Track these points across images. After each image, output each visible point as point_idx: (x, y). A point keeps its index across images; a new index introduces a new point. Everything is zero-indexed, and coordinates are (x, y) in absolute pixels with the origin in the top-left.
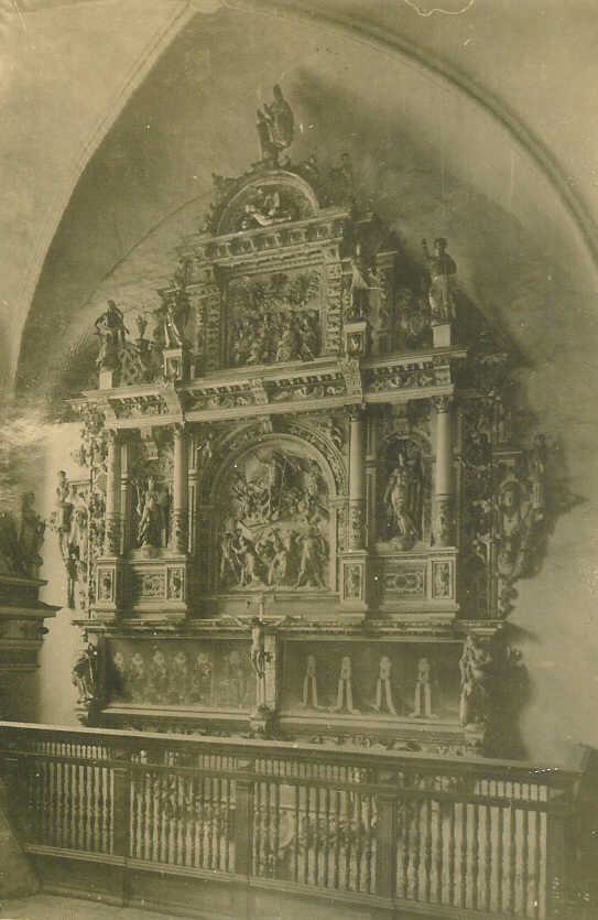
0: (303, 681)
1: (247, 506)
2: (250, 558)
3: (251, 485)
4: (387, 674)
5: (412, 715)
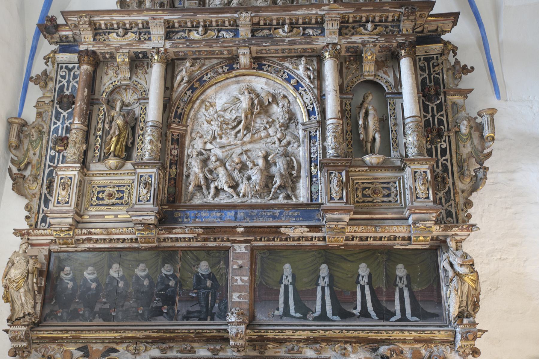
0: (394, 293)
1: (218, 130)
2: (221, 171)
3: (222, 113)
4: (366, 279)
5: (393, 319)
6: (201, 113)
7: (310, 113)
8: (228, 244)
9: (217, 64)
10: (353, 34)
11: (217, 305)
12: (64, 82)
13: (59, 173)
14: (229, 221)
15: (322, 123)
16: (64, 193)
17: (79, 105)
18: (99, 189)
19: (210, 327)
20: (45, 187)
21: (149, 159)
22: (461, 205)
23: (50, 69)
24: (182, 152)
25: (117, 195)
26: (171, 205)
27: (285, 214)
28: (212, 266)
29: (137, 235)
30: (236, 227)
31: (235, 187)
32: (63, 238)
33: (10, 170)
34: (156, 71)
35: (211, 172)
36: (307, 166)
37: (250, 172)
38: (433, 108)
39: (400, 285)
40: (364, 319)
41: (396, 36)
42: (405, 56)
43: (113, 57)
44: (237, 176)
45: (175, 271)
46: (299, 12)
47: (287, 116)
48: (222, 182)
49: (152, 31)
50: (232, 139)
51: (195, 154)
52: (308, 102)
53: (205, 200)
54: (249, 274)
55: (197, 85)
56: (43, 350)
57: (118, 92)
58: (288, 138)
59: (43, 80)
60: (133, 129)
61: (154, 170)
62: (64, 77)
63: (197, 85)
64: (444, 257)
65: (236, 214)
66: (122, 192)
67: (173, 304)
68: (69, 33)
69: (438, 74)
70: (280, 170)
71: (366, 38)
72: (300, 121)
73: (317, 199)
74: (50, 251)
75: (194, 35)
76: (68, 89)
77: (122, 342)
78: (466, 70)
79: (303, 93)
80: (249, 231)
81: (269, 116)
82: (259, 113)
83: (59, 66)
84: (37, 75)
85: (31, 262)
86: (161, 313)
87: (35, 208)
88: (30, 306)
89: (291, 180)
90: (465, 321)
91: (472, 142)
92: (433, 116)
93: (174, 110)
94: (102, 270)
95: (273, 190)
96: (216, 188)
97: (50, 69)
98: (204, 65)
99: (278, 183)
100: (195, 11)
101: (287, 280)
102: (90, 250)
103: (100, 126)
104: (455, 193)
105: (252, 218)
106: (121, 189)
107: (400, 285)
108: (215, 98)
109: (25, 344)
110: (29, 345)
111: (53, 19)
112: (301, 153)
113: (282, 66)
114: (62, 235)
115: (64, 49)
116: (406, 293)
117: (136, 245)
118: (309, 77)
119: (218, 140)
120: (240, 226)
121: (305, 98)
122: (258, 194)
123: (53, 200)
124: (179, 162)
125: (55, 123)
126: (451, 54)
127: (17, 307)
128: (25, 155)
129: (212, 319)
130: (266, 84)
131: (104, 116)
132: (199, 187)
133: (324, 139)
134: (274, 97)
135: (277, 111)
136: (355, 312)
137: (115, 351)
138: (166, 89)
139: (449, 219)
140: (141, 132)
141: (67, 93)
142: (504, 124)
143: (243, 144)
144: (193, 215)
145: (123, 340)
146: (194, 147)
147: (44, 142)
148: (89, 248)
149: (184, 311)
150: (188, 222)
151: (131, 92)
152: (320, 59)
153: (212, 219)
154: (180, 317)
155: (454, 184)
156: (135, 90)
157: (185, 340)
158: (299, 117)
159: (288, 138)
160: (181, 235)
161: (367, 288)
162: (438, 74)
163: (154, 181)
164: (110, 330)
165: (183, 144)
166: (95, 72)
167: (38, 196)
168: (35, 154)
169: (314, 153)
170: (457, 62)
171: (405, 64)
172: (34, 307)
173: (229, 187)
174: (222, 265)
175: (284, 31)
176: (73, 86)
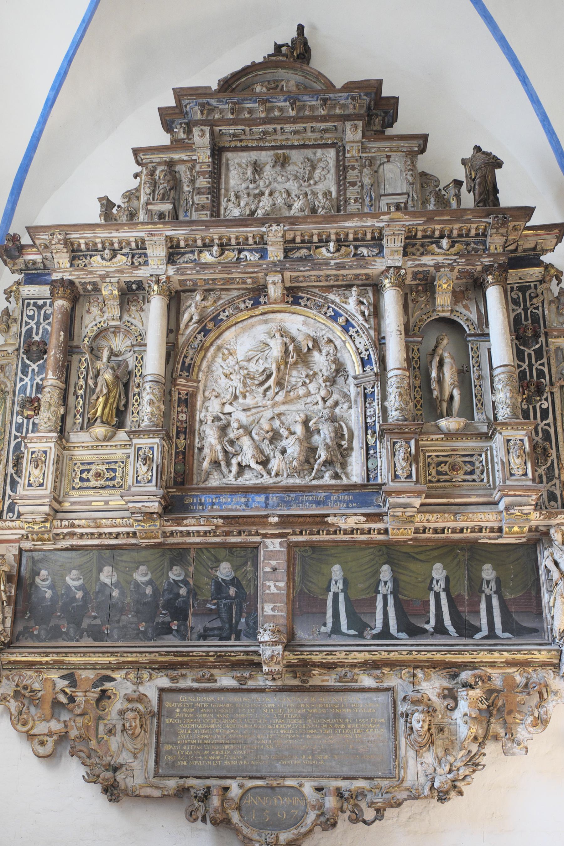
1: (240, 386)
2: (246, 442)
3: (245, 364)
4: (442, 584)
5: (478, 636)
7: (364, 363)
8: (258, 539)
9: (238, 297)
10: (422, 254)
11: (243, 620)
12: (33, 324)
14: (258, 509)
15: (382, 375)
16: (36, 472)
17: (53, 354)
18: (82, 467)
20: (11, 465)
23: (14, 307)
24: (192, 417)
25: (107, 475)
26: (179, 491)
27: (333, 498)
28: (236, 568)
29: (136, 528)
30: (267, 516)
32: (37, 533)
34: (156, 307)
35: (232, 443)
36: (362, 434)
37: (284, 443)
38: (529, 355)
39: (487, 591)
41: (481, 256)
42: (493, 284)
43: (97, 289)
44: (267, 448)
45: (186, 575)
46: (349, 224)
47: (333, 367)
48: (248, 456)
50: (259, 398)
51: (210, 419)
52: (361, 347)
53: (225, 481)
55: (211, 325)
57: (104, 337)
58: (335, 397)
60: (126, 386)
61: (157, 440)
62: (31, 317)
63: (210, 326)
65: (267, 499)
67: (186, 618)
71: (440, 259)
72: (351, 373)
74: (20, 550)
76: (37, 334)
77: (119, 669)
79: (355, 335)
80: (285, 521)
81: (309, 367)
82: (296, 363)
83: (25, 303)
86: (169, 631)
89: (340, 453)
92: (530, 366)
93: (181, 361)
94: (90, 574)
95: (316, 467)
96: (239, 464)
97: (14, 307)
98: (219, 298)
99: (323, 458)
100: (208, 225)
101: (337, 587)
102: (73, 548)
103: (82, 382)
105: (288, 504)
106: (113, 466)
107: (487, 591)
112: (354, 418)
113: (326, 299)
114: (36, 528)
115: (31, 280)
116: (495, 602)
118: (363, 313)
119: (241, 400)
120: (273, 515)
121: (357, 342)
122: (297, 472)
123: (22, 482)
124: (188, 430)
125: (22, 380)
126: (554, 281)
129: (238, 638)
130: (304, 323)
132: (216, 463)
133: (384, 397)
134: (315, 341)
135: (321, 361)
136: (427, 627)
137: (113, 680)
140: (136, 390)
141: (37, 338)
143: (274, 405)
144: (209, 500)
145: (120, 666)
146: (208, 409)
147: (8, 405)
148: (72, 546)
149: (200, 628)
150: (203, 510)
151: (122, 336)
152: (378, 289)
153: (235, 506)
154: (195, 636)
156: (127, 333)
157: (202, 665)
159: (335, 397)
160: (194, 528)
162: (537, 308)
163: (157, 456)
164: (103, 653)
165: (194, 406)
166: (73, 309)
169: (371, 416)
171: (493, 294)
174: (249, 567)
175: (328, 250)
176: (45, 330)
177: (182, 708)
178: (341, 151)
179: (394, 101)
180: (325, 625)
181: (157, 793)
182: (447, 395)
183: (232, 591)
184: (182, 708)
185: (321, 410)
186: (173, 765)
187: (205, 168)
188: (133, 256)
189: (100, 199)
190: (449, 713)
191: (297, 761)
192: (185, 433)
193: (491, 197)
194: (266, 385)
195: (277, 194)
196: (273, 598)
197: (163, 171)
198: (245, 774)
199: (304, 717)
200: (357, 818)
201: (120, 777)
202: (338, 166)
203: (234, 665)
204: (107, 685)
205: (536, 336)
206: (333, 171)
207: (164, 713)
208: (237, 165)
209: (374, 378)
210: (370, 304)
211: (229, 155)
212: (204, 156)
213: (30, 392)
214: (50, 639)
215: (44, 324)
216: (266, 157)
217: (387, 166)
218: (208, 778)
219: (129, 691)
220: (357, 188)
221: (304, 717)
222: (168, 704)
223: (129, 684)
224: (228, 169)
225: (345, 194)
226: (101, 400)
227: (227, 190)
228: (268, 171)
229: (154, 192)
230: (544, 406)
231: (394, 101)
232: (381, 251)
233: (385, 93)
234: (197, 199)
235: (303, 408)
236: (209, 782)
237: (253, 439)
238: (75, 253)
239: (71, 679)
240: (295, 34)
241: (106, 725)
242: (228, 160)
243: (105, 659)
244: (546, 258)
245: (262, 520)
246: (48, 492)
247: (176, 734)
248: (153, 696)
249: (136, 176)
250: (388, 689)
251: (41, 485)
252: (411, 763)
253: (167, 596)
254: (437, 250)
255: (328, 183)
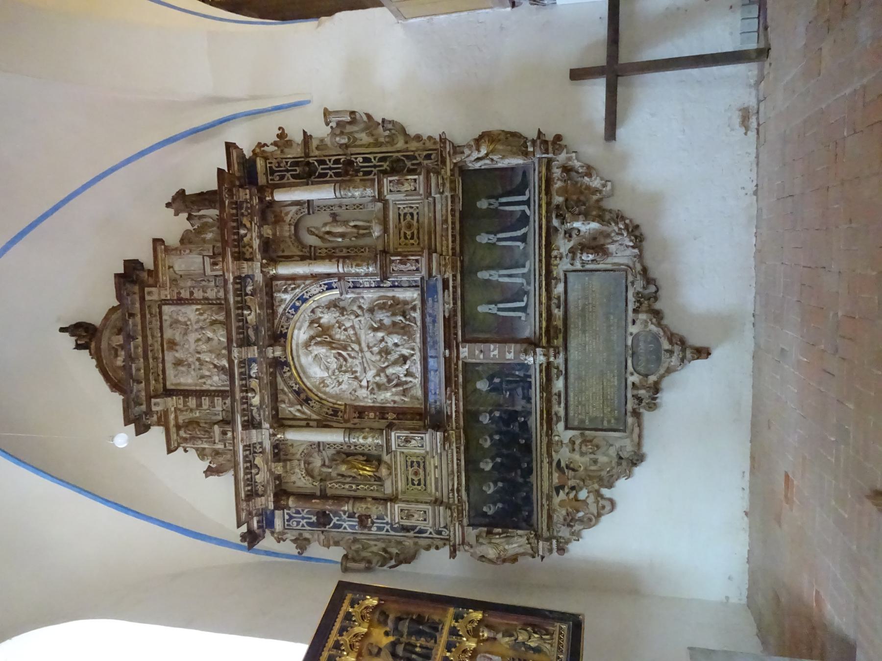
1: (347, 375)
2: (390, 371)
6: (331, 391)
7: (330, 288)
8: (460, 363)
9: (282, 377)
10: (251, 247)
11: (517, 373)
12: (303, 522)
13: (397, 521)
14: (439, 363)
15: (340, 277)
16: (416, 516)
17: (328, 506)
18: (410, 484)
19: (536, 379)
20: (407, 534)
21: (382, 440)
22: (419, 145)
23: (290, 535)
24: (372, 408)
25: (416, 467)
26: (426, 418)
27: (431, 311)
28: (480, 378)
29: (454, 446)
30: (445, 357)
31: (404, 359)
32: (458, 514)
33: (391, 567)
34: (291, 436)
35: (390, 381)
36: (383, 290)
37: (390, 344)
38: (322, 169)
39: (496, 205)
40: (528, 239)
41: (252, 205)
42: (273, 197)
43: (278, 478)
44: (393, 357)
45: (485, 412)
46: (232, 301)
47: (333, 309)
48: (400, 370)
49: (254, 440)
50: (357, 362)
51: (373, 396)
52: (319, 289)
53: (418, 386)
54: (487, 344)
55: (303, 396)
56: (559, 525)
57: (312, 471)
58: (355, 308)
59: (302, 543)
60: (348, 455)
61: (393, 434)
62: (298, 523)
63: (303, 396)
64: (470, 165)
65: (431, 357)
66: (412, 462)
67: (516, 412)
68: (255, 520)
69: (287, 162)
70: (388, 316)
71: (254, 235)
72: (339, 296)
73: (416, 281)
74: (468, 525)
75: (256, 401)
76: (310, 518)
77: (551, 456)
78: (282, 135)
79: (309, 294)
80: (448, 345)
81: (333, 326)
82: (330, 336)
83: (287, 528)
84: (297, 548)
85: (481, 540)
86: (525, 423)
87: (428, 541)
88: (520, 539)
89: (398, 307)
90: (531, 149)
91: (357, 132)
92: (330, 169)
93: (331, 416)
94: (486, 477)
95: (408, 323)
96: (406, 376)
97: (290, 535)
98: (283, 390)
99: (401, 318)
100: (233, 400)
101: (493, 309)
102: (467, 490)
103: (347, 486)
104: (407, 150)
105: (435, 343)
106: (409, 463)
107: (496, 205)
108: (315, 378)
109: (554, 541)
110: (555, 538)
111: (243, 537)
112: (369, 296)
113: (282, 315)
114: (455, 515)
115: (270, 524)
116: (504, 200)
117: (462, 448)
118: (293, 289)
119: (358, 374)
120: (444, 353)
121: (315, 293)
122: (411, 336)
123: (421, 525)
124: (382, 411)
125: (345, 528)
126: (266, 148)
127: (522, 550)
128: (376, 554)
129: (530, 376)
130: (300, 329)
131: (337, 483)
132: (405, 393)
133: (357, 275)
134: (312, 322)
135: (327, 318)
136: (521, 248)
137: (559, 462)
138: (308, 426)
139: (433, 157)
140: (352, 448)
141: (314, 519)
142: (338, 101)
143: (361, 351)
144: (433, 397)
145: (550, 456)
146: (365, 397)
147: (363, 537)
148: (466, 490)
149: (523, 402)
150: (440, 401)
151: (311, 459)
152: (276, 277)
153: (437, 379)
154: (528, 406)
155: (398, 152)
156: (309, 455)
157: (549, 401)
158: (333, 298)
159: (355, 308)
160: (453, 407)
161: (500, 236)
162: (287, 162)
163: (404, 434)
164: (541, 468)
165: (363, 407)
166: (293, 494)
167: (417, 540)
168: (376, 545)
169: (370, 283)
170: (275, 144)
171: (281, 196)
172: (521, 536)
173: (405, 363)
174: (480, 368)
175: (249, 315)
176: (308, 513)
177: (579, 414)
178: (166, 302)
179: (127, 263)
180: (520, 317)
181: (636, 430)
182: (355, 230)
183: (497, 380)
184: (579, 414)
185: (365, 319)
186: (617, 419)
187: (181, 401)
188: (255, 452)
189: (207, 477)
190: (582, 234)
191: (615, 338)
192: (384, 414)
193: (207, 197)
194: (347, 356)
195: (199, 349)
196: (502, 353)
197: (185, 432)
198: (623, 370)
199: (584, 332)
200: (655, 297)
201: (624, 455)
202: (177, 304)
203: (549, 379)
204: (563, 464)
205: (308, 164)
206: (179, 307)
207: (582, 426)
208: (177, 378)
209: (342, 282)
210: (285, 284)
211: (168, 384)
212: (172, 402)
213: (354, 522)
214: (532, 503)
215: (304, 514)
216: (169, 357)
217: (176, 268)
218: (626, 397)
219: (567, 450)
220: (195, 291)
221: (584, 332)
222: (576, 423)
223: (562, 450)
224: (179, 384)
225: (200, 300)
226: (361, 472)
227: (196, 385)
228: (179, 355)
229: (200, 438)
230: (361, 160)
231: (127, 263)
232: (248, 276)
233: (121, 270)
234: (205, 407)
235: (363, 331)
236: (629, 395)
237: (387, 366)
238: (252, 495)
239: (558, 489)
240: (67, 334)
241: (590, 465)
242: (172, 384)
243: (546, 465)
244: (248, 154)
245: (448, 361)
246: (430, 507)
247: (596, 417)
248: (571, 433)
249: (186, 451)
250: (565, 275)
251: (425, 512)
252: (616, 260)
253: (501, 424)
254: (249, 236)
255: (190, 313)
